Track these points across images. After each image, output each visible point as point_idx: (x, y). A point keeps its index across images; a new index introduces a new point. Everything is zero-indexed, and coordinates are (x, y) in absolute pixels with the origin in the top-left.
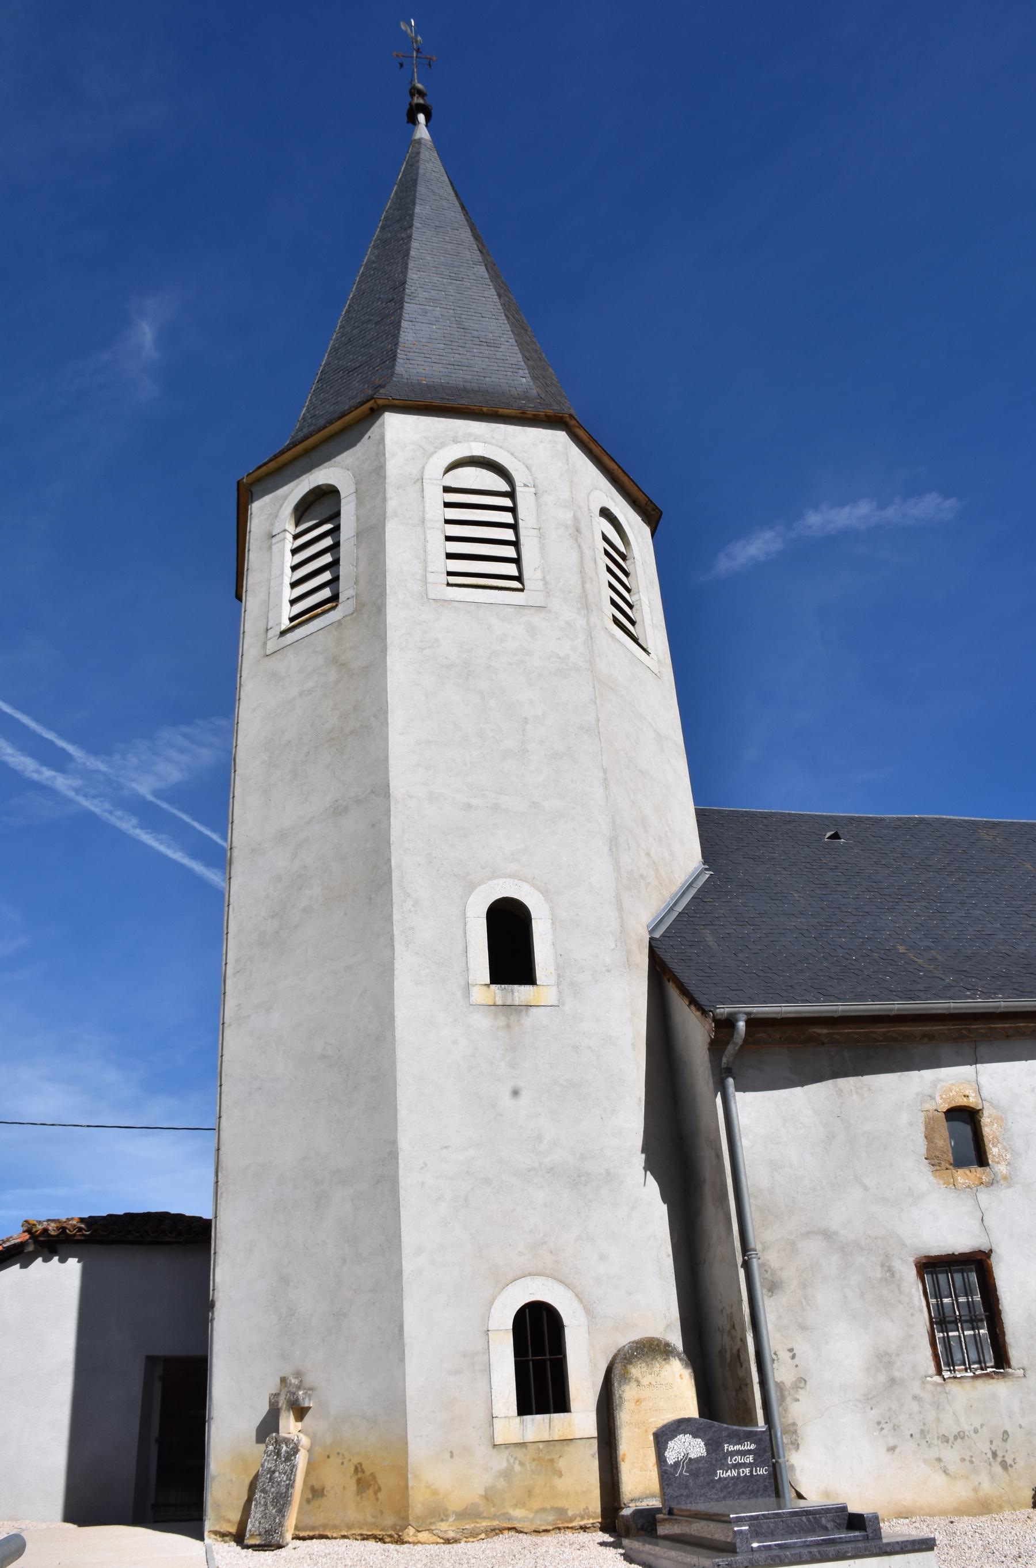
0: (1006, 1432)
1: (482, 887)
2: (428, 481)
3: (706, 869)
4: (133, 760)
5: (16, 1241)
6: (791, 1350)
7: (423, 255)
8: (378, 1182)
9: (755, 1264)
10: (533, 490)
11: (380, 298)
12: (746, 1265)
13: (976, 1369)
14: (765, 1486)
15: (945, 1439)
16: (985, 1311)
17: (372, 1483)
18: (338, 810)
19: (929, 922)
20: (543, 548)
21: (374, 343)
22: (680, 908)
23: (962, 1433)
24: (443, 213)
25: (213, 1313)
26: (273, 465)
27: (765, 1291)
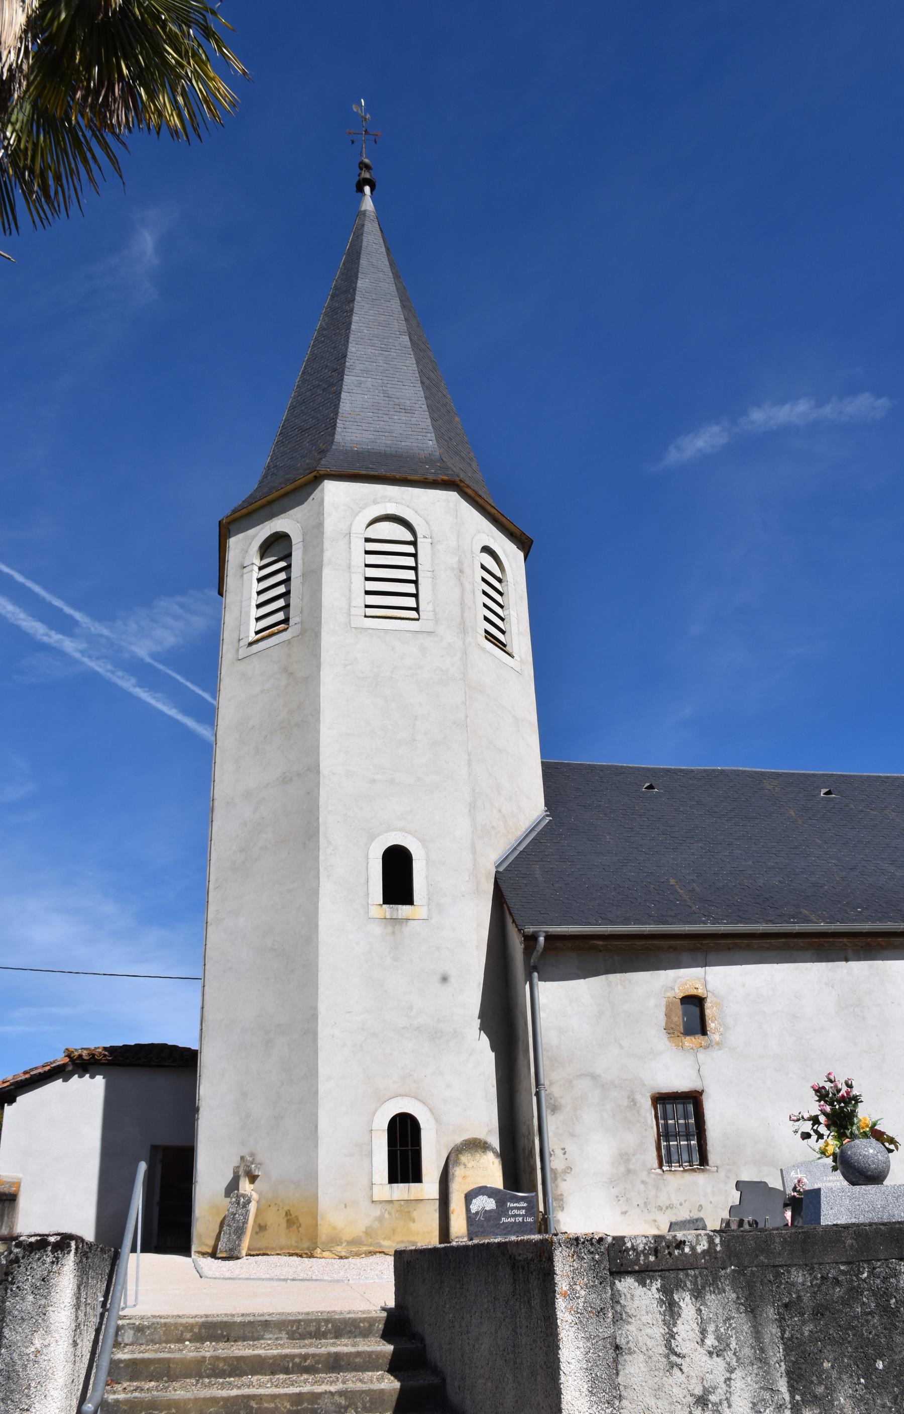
0: (701, 1206)
1: (380, 837)
2: (354, 535)
3: (547, 816)
4: (133, 626)
5: (60, 1063)
6: (563, 1149)
7: (362, 328)
8: (305, 1033)
9: (543, 1093)
10: (429, 540)
11: (327, 366)
12: (538, 1094)
13: (686, 1166)
14: (532, 1229)
15: (660, 1208)
16: (696, 1129)
17: (296, 1221)
18: (285, 780)
19: (700, 859)
20: (434, 586)
21: (321, 408)
22: (521, 848)
23: (671, 1206)
24: (379, 285)
25: (198, 1115)
26: (244, 511)
27: (549, 1111)
